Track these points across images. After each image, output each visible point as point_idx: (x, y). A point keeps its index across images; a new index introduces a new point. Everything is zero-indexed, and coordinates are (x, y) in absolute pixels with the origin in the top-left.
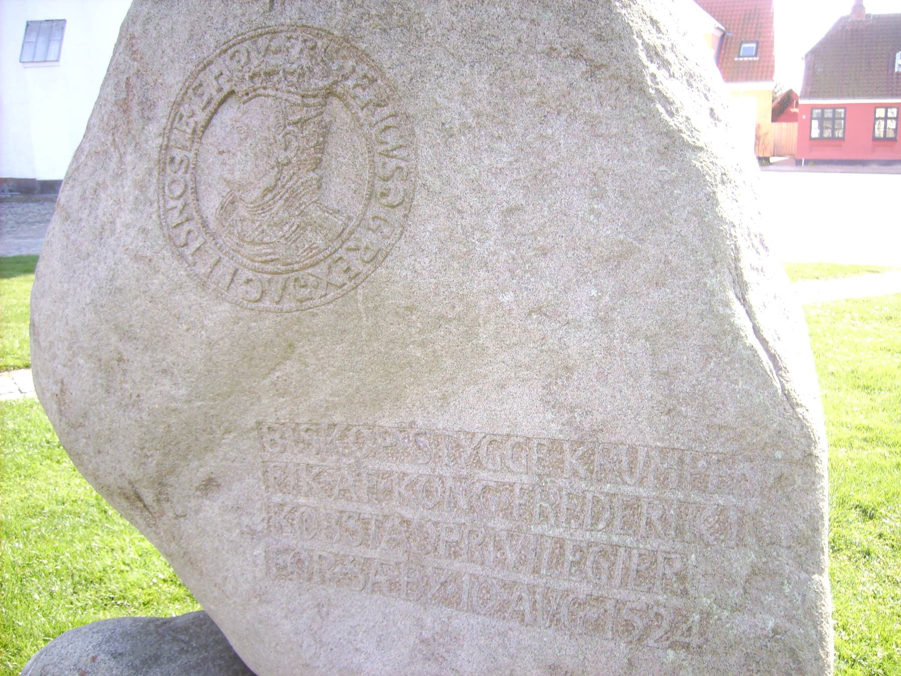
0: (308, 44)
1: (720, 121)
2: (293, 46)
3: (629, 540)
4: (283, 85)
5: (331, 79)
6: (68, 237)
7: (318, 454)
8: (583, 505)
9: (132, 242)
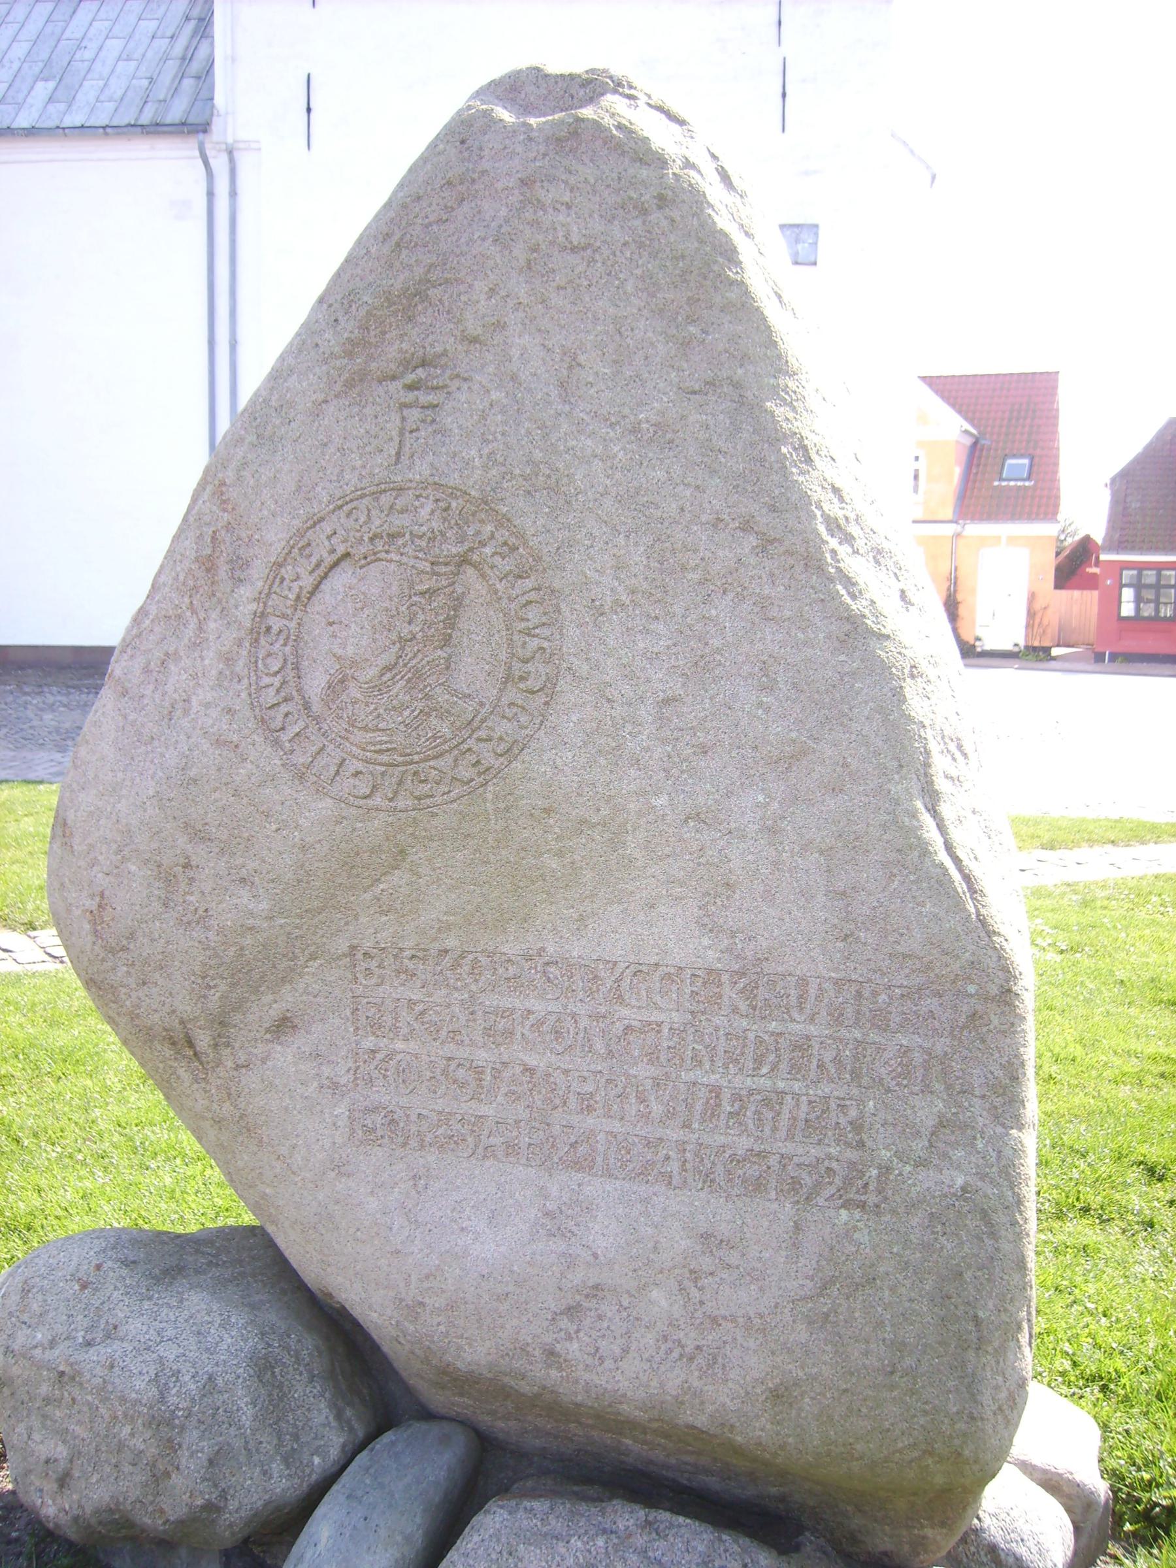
0: (440, 504)
1: (913, 605)
2: (422, 506)
3: (797, 1086)
4: (409, 550)
5: (467, 545)
6: (125, 717)
7: (423, 987)
8: (744, 1047)
9: (212, 726)
